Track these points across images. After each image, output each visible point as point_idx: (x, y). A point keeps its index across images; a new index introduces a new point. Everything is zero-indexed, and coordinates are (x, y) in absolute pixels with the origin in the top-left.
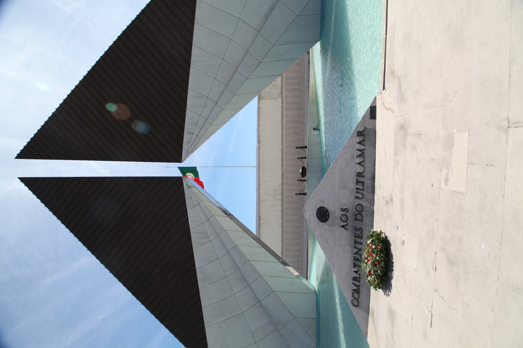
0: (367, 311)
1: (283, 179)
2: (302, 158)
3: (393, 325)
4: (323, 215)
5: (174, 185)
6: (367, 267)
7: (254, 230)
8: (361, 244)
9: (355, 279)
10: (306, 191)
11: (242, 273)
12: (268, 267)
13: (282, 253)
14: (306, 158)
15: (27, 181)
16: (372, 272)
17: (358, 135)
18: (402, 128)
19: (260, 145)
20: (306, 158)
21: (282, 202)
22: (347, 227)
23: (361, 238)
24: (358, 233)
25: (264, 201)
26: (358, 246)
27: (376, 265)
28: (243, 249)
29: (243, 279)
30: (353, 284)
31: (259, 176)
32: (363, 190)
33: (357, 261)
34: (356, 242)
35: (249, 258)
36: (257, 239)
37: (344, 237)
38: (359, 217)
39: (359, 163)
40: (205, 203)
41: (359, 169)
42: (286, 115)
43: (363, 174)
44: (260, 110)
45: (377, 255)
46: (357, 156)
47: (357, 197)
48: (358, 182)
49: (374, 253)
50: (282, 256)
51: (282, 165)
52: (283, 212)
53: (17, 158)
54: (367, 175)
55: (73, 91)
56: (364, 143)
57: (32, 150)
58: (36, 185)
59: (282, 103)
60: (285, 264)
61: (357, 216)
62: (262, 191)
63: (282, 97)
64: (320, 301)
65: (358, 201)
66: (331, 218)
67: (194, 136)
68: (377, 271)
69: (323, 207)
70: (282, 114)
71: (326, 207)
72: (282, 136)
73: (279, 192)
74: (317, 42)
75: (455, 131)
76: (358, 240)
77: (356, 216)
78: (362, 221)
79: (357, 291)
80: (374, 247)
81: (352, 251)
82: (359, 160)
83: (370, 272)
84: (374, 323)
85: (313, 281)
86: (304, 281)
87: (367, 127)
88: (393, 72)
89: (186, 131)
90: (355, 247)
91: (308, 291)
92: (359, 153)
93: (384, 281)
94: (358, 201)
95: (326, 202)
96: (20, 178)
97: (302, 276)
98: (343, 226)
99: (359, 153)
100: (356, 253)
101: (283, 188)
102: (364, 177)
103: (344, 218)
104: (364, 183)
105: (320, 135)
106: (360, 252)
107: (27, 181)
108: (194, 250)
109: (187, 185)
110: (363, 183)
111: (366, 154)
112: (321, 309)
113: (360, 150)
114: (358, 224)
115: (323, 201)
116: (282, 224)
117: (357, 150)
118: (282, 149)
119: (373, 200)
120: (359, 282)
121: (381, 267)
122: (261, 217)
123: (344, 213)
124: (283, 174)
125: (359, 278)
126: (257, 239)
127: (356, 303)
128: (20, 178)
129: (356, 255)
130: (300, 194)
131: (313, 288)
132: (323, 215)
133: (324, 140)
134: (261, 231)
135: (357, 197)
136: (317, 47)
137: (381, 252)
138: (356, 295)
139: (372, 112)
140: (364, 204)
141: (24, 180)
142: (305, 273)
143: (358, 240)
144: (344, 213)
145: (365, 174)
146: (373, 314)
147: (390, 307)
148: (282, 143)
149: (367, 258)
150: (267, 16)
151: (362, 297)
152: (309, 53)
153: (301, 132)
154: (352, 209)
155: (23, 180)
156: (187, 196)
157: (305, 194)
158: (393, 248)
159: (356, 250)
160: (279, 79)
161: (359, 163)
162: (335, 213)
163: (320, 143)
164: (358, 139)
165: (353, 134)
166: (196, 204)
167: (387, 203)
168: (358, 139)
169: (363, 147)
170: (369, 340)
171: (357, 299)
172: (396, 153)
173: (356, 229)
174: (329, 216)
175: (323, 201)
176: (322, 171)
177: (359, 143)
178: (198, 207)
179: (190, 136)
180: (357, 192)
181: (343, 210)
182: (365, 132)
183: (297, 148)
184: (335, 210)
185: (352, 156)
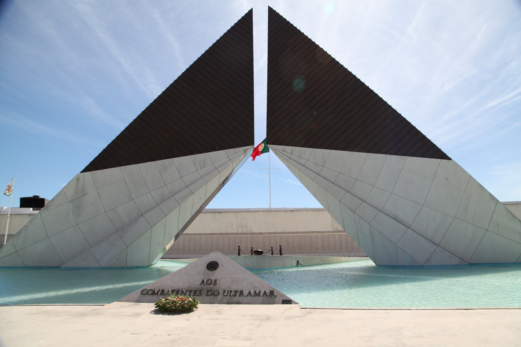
0: (138, 301)
1: (257, 234)
2: (272, 251)
3: (130, 316)
4: (213, 266)
5: (247, 138)
6: (172, 298)
7: (209, 206)
8: (190, 295)
9: (163, 291)
10: (242, 256)
11: (168, 200)
12: (174, 222)
13: (187, 234)
14: (272, 254)
15: (249, 16)
16: (168, 301)
17: (271, 291)
18: (268, 318)
19: (289, 212)
20: (272, 254)
21: (236, 234)
22: (202, 285)
23: (194, 295)
24: (198, 293)
25: (237, 217)
26: (188, 293)
27: (173, 303)
28: (190, 200)
29: (163, 200)
30: (159, 290)
31: (259, 211)
32: (230, 296)
33: (176, 292)
34: (191, 291)
35: (182, 205)
36: (199, 211)
37: (195, 282)
38: (210, 293)
39: (250, 293)
40: (231, 166)
41: (246, 293)
42: (317, 236)
43: (241, 295)
44: (321, 211)
45: (180, 304)
46: (255, 291)
47: (224, 291)
48: (236, 292)
49: (182, 302)
50: (185, 234)
51: (270, 233)
52: (226, 234)
53: (269, 7)
54: (241, 299)
55: (326, 53)
56: (265, 296)
57: (275, 20)
58: (246, 23)
59: (328, 232)
60: (177, 237)
61: (210, 291)
62: (246, 214)
63: (334, 232)
64: (143, 269)
65: (221, 292)
66: (210, 272)
67: (289, 155)
68: (168, 304)
69: (218, 266)
70: (318, 232)
71: (218, 268)
72: (297, 233)
73: (245, 231)
74: (375, 262)
75: (253, 341)
76: (192, 293)
77: (211, 291)
78: (207, 295)
79: (153, 293)
80: (186, 302)
81: (184, 289)
82: (252, 292)
83: (168, 299)
84: (129, 305)
85: (159, 264)
86: (161, 255)
87: (277, 298)
88: (310, 313)
89: (294, 148)
90: (187, 291)
91: (151, 259)
92: (257, 292)
93: (163, 310)
94: (221, 292)
95: (222, 268)
96: (252, 9)
97: (165, 254)
98: (203, 281)
99: (257, 292)
100: (182, 291)
101: (249, 234)
102: (240, 296)
103: (209, 282)
104: (235, 297)
105: (292, 267)
106: (183, 294)
107: (249, 16)
108: (189, 156)
109: (247, 149)
110: (235, 295)
111: (256, 297)
112: (135, 270)
113: (259, 293)
114: (204, 292)
115: (223, 266)
116: (215, 234)
117: (260, 291)
118: (285, 233)
119: (222, 303)
120: (161, 295)
121: (171, 307)
122: (221, 214)
123: (213, 282)
124: (261, 234)
125: (164, 294)
126: (199, 211)
127: (145, 292)
128: (252, 9)
129: (181, 292)
130: (239, 250)
131: (153, 263)
132: (213, 266)
133: (287, 270)
134: (208, 214)
135: (224, 291)
136: (370, 263)
137: (183, 307)
138: (150, 292)
139: (288, 302)
140: (219, 297)
141: (250, 13)
142: (169, 256)
143: (192, 293)
144: (213, 282)
145: (242, 297)
146: (136, 305)
147: (142, 314)
148: (290, 233)
149: (178, 297)
150: (396, 219)
151: (149, 297)
152: (367, 256)
153: (293, 251)
154: (215, 288)
155: (251, 12)
156: (237, 149)
157: (239, 254)
158: (185, 315)
159: (184, 291)
160: (340, 228)
161: (250, 293)
162: (214, 275)
163: (284, 267)
164: (268, 292)
165: (272, 287)
166: (230, 158)
167: (218, 311)
168: (268, 292)
169: (261, 295)
170: (115, 303)
171: (147, 293)
172: (252, 315)
173: (201, 291)
174: (212, 270)
175: (223, 266)
176: (256, 270)
177: (265, 292)
178: (228, 159)
179: (290, 151)
180: (228, 291)
181: (215, 281)
182: (273, 296)
183: (280, 246)
184: (216, 275)
185: (255, 287)
